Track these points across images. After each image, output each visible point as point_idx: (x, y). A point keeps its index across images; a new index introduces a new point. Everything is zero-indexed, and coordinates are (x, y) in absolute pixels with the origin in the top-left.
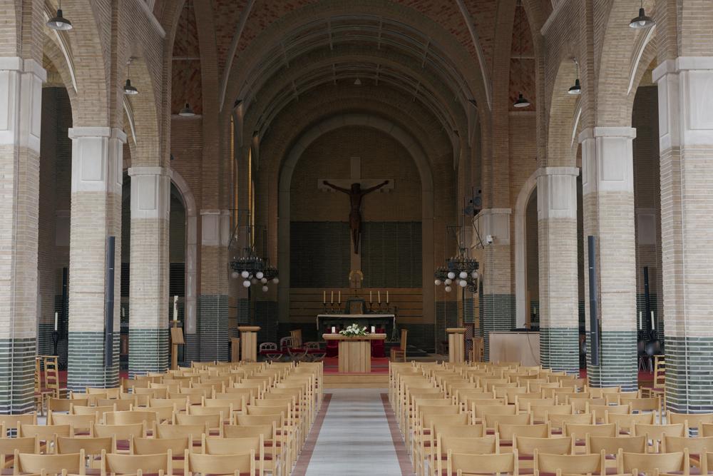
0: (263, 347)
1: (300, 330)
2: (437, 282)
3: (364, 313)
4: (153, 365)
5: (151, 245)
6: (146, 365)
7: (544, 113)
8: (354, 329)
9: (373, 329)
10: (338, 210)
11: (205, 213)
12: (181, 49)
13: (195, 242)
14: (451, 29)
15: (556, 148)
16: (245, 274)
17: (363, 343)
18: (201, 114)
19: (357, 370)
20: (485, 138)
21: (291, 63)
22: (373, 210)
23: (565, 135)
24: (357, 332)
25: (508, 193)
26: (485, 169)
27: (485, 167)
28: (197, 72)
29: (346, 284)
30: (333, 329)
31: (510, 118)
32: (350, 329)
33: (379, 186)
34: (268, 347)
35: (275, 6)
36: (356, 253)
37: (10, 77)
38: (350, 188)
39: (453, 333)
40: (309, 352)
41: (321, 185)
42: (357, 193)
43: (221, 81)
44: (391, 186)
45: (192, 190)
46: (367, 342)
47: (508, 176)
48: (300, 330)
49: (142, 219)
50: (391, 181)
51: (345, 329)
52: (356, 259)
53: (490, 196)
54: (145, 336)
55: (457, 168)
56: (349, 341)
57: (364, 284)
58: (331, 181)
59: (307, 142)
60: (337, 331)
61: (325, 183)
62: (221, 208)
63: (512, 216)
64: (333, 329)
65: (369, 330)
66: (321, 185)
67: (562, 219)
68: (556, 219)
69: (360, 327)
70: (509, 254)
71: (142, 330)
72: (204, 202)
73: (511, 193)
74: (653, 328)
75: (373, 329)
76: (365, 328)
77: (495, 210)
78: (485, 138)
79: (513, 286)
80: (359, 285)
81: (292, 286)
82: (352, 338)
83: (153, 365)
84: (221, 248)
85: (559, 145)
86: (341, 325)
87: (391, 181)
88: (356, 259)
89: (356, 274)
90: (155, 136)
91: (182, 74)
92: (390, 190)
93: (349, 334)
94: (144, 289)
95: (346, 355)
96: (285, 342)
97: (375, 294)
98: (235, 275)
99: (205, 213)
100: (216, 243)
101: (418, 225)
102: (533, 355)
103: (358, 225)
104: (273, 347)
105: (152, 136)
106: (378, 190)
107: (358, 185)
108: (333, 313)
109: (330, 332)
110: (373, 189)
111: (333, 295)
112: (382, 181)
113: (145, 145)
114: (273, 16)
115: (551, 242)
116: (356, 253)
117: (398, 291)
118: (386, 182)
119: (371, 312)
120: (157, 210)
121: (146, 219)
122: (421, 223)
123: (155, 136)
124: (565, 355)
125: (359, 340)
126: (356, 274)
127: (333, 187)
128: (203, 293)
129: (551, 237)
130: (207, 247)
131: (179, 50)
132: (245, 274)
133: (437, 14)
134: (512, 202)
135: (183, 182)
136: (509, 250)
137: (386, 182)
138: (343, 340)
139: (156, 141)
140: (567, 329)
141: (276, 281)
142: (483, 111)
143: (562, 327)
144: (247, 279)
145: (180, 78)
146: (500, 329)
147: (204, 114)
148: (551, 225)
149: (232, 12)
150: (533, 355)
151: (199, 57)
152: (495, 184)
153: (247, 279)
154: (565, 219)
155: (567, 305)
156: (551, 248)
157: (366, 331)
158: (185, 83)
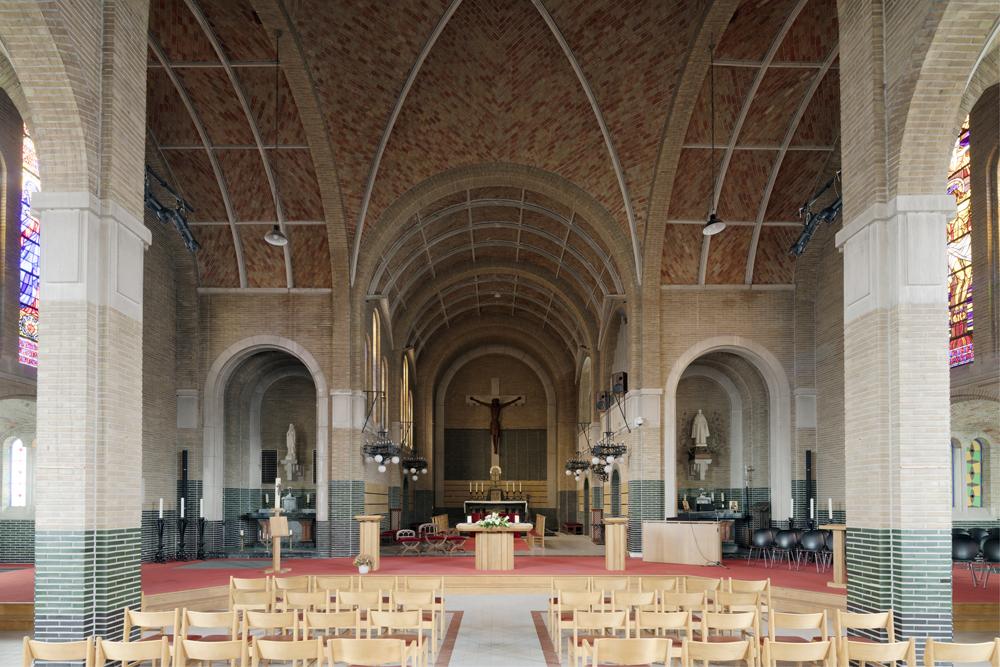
0: (401, 535)
1: (446, 516)
2: (568, 472)
3: (502, 500)
4: (75, 606)
5: (71, 357)
6: (60, 605)
7: (882, 94)
8: (494, 520)
9: (517, 518)
10: (482, 421)
11: (335, 392)
12: (304, 210)
13: (326, 424)
14: (599, 196)
15: (918, 157)
16: (379, 458)
17: (505, 535)
18: (330, 286)
19: (498, 568)
20: (634, 315)
21: (451, 321)
22: (509, 421)
23: (939, 125)
24: (497, 523)
25: (658, 372)
26: (634, 348)
27: (634, 345)
28: (325, 240)
29: (487, 477)
30: (469, 518)
31: (662, 293)
32: (489, 519)
33: (513, 402)
34: (406, 534)
35: (409, 168)
36: (496, 453)
37: (81, 219)
38: (491, 402)
39: (613, 523)
40: (448, 539)
41: (468, 400)
42: (496, 407)
43: (351, 251)
44: (523, 401)
45: (322, 369)
46: (509, 535)
47: (658, 355)
48: (446, 516)
49: (53, 303)
50: (523, 397)
51: (484, 519)
52: (495, 458)
53: (639, 377)
54: (59, 545)
55: (578, 382)
56: (488, 532)
57: (502, 477)
58: (475, 397)
59: (457, 366)
60: (474, 521)
61: (472, 399)
62: (353, 388)
63: (662, 397)
64: (469, 518)
65: (512, 520)
66: (468, 400)
67: (926, 305)
68: (914, 305)
69: (502, 515)
70: (659, 438)
71: (51, 533)
72: (334, 382)
73: (662, 373)
74: (812, 517)
75: (517, 518)
76: (507, 518)
77: (644, 391)
78: (634, 315)
79: (662, 472)
80: (498, 478)
81: (446, 479)
82: (491, 530)
83: (75, 606)
84: (353, 431)
85: (922, 151)
86: (480, 512)
87: (523, 397)
88: (495, 458)
89: (496, 468)
90: (74, 125)
91: (310, 243)
92: (523, 405)
93: (488, 524)
94: (57, 449)
95: (485, 550)
96: (423, 529)
97: (509, 485)
98: (405, 471)
99: (335, 392)
100: (348, 425)
101: (544, 432)
102: (698, 548)
103: (497, 432)
104: (411, 534)
105: (69, 125)
106: (513, 404)
107: (497, 400)
108: (477, 499)
109: (465, 521)
110: (509, 403)
111: (479, 485)
112: (515, 397)
113: (57, 160)
114: (408, 181)
115: (903, 353)
116: (496, 453)
117: (529, 483)
118: (519, 398)
119: (507, 499)
120: (85, 284)
121: (61, 303)
122: (545, 430)
123: (74, 125)
124: (930, 587)
125: (501, 532)
126: (496, 468)
127: (478, 401)
128: (334, 478)
129: (903, 342)
130: (338, 429)
131: (303, 213)
132: (413, 470)
133: (584, 178)
134: (662, 383)
135: (313, 360)
136: (659, 434)
137: (519, 398)
138: (481, 532)
139: (78, 137)
140: (936, 532)
141: (424, 471)
142: (632, 285)
143: (926, 528)
144: (415, 474)
145: (308, 247)
146: (649, 518)
147: (334, 286)
148: (903, 317)
149: (359, 164)
150: (698, 548)
151: (324, 220)
152: (644, 363)
153: (415, 474)
154: (933, 305)
155: (935, 483)
156: (903, 365)
157: (509, 521)
158: (313, 254)
